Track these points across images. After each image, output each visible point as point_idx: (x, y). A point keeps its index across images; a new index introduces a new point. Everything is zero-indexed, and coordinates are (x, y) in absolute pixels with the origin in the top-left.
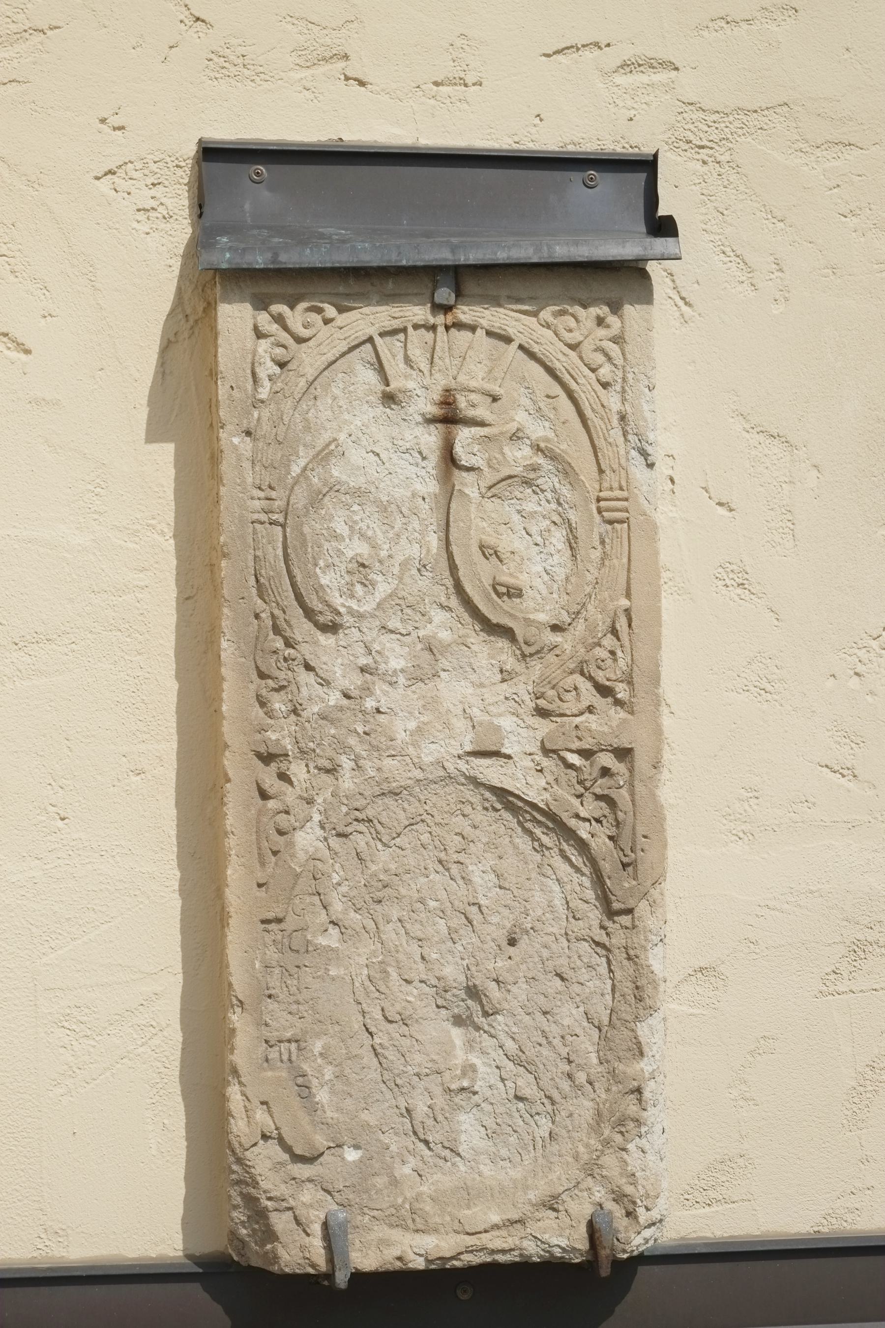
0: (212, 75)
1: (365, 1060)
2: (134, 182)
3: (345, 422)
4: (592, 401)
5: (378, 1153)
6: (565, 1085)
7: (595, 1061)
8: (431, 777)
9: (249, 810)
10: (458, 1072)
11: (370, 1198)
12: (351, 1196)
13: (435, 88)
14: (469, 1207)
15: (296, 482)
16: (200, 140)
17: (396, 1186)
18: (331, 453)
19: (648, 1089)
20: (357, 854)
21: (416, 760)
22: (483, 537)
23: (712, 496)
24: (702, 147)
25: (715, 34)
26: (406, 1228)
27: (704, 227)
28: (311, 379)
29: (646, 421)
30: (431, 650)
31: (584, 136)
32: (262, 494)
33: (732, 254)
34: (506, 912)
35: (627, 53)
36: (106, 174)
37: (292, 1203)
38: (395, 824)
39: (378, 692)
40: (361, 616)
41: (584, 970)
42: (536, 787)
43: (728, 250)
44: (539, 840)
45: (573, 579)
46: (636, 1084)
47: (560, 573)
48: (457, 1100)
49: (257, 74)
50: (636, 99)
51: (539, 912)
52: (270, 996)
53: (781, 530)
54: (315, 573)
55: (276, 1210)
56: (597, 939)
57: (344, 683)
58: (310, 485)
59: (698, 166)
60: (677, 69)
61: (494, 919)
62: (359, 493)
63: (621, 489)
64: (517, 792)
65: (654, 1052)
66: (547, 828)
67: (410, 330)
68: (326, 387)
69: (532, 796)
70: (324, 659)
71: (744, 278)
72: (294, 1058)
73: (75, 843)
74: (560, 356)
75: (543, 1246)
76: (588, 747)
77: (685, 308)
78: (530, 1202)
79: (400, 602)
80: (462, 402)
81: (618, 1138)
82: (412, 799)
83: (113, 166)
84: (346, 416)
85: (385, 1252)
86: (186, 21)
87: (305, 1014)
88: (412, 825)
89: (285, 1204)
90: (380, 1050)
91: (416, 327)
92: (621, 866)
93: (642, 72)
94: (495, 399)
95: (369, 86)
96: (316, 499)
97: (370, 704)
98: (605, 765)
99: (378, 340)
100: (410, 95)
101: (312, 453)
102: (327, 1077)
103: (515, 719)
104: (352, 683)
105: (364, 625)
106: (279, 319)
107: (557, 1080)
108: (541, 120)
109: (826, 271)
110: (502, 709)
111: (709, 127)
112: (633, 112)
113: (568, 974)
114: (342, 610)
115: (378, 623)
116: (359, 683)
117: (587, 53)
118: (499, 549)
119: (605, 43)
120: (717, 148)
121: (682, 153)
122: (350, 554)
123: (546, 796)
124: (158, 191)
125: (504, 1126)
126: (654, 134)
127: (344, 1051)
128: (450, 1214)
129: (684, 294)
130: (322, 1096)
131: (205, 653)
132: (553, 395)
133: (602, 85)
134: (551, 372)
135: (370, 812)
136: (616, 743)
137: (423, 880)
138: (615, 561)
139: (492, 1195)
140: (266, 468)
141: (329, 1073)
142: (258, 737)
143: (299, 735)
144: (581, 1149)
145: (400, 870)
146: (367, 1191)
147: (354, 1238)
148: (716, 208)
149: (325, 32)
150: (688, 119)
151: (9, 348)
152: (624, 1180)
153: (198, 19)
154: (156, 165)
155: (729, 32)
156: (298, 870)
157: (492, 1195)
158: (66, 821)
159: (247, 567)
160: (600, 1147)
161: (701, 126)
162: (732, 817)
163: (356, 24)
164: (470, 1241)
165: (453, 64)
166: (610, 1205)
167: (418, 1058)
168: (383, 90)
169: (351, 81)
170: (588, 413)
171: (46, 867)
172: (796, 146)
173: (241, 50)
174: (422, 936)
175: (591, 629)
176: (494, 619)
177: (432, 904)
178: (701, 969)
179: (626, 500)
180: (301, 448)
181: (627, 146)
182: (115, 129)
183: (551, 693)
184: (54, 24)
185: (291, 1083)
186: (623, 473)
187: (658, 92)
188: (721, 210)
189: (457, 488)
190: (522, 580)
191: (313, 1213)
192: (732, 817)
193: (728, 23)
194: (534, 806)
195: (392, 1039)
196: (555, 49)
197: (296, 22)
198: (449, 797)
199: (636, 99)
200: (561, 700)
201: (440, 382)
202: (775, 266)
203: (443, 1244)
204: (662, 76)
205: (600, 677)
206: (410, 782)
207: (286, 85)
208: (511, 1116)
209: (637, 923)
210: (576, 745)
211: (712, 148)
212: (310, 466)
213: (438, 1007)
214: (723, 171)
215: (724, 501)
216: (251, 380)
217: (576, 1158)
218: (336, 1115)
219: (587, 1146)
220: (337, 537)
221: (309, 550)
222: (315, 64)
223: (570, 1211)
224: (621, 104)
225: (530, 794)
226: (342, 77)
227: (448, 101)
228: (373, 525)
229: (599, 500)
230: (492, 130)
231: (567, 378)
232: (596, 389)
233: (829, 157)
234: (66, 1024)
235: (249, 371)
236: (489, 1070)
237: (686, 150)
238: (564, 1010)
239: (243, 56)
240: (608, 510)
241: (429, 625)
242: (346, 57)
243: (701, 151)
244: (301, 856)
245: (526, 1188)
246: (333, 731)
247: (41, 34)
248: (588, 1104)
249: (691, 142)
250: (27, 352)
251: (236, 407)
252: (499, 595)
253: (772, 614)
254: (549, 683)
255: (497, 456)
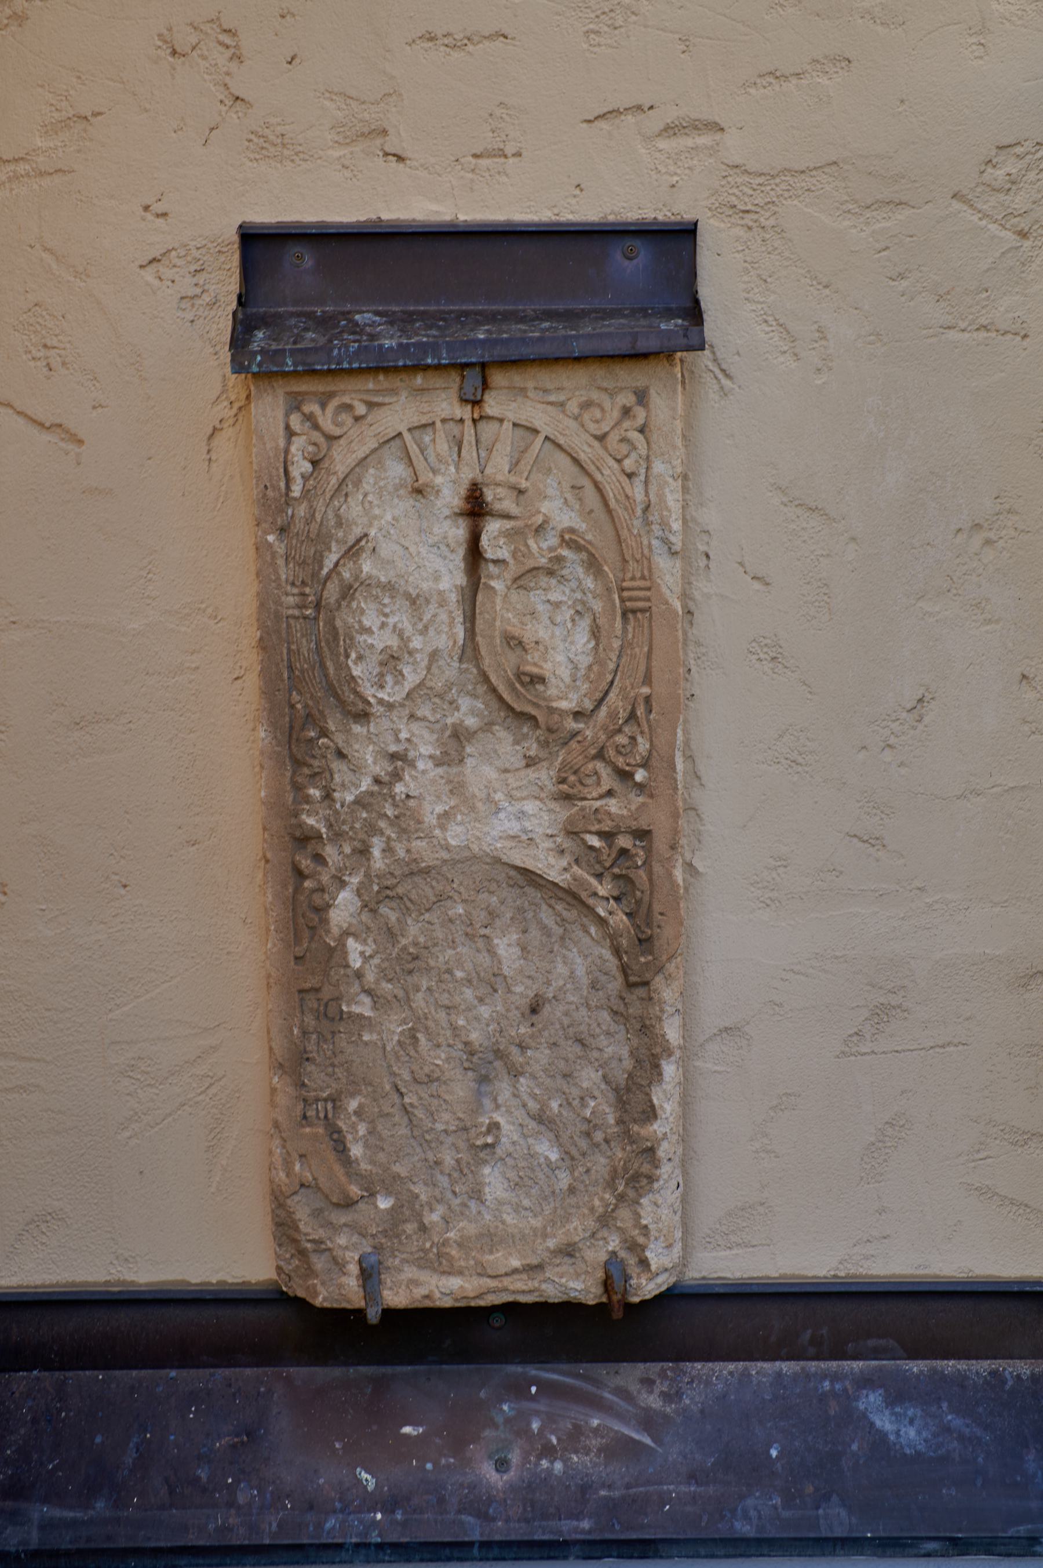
0: (252, 156)
1: (397, 1119)
2: (178, 270)
3: (375, 517)
4: (616, 493)
5: (409, 1202)
6: (583, 1144)
7: (612, 1121)
8: (457, 857)
9: (287, 889)
10: (484, 1129)
11: (400, 1242)
12: (383, 1241)
13: (473, 161)
14: (491, 1252)
15: (328, 577)
16: (240, 227)
17: (425, 1232)
18: (362, 549)
19: (662, 1149)
20: (389, 929)
21: (443, 842)
22: (509, 628)
23: (748, 570)
24: (748, 212)
25: (762, 91)
26: (435, 1270)
27: (747, 295)
28: (341, 476)
29: (670, 511)
30: (458, 737)
31: (625, 205)
32: (295, 591)
33: (774, 323)
34: (529, 982)
35: (671, 115)
36: (150, 262)
37: (329, 1244)
38: (424, 901)
39: (407, 777)
40: (390, 706)
41: (602, 1037)
42: (557, 867)
43: (770, 319)
44: (560, 915)
45: (595, 668)
46: (649, 1144)
47: (585, 661)
48: (482, 1155)
49: (297, 154)
50: (679, 163)
51: (561, 983)
52: (308, 1059)
53: (817, 604)
54: (347, 665)
55: (315, 1251)
56: (615, 1008)
57: (377, 770)
58: (342, 580)
59: (741, 232)
60: (722, 129)
61: (519, 989)
62: (389, 588)
63: (643, 578)
64: (539, 872)
65: (668, 1114)
66: (568, 904)
67: (438, 424)
68: (358, 483)
69: (554, 876)
70: (356, 747)
71: (786, 348)
72: (330, 1115)
73: (136, 909)
74: (586, 448)
75: (560, 1289)
76: (607, 829)
77: (725, 382)
78: (548, 1249)
79: (429, 692)
80: (489, 495)
81: (631, 1194)
82: (440, 877)
83: (157, 254)
84: (377, 511)
85: (415, 1291)
86: (227, 102)
87: (340, 1075)
88: (440, 901)
89: (323, 1246)
90: (410, 1109)
91: (444, 421)
92: (637, 942)
93: (686, 134)
94: (521, 492)
95: (408, 162)
96: (347, 592)
97: (399, 789)
98: (624, 846)
99: (407, 436)
100: (449, 169)
101: (344, 548)
102: (361, 1133)
103: (538, 803)
104: (382, 769)
105: (394, 715)
106: (310, 418)
107: (576, 1138)
108: (582, 190)
109: (872, 338)
110: (525, 793)
111: (754, 190)
112: (676, 178)
113: (589, 1041)
114: (372, 700)
115: (407, 712)
116: (390, 769)
117: (630, 117)
118: (524, 640)
119: (649, 105)
120: (762, 212)
121: (726, 220)
122: (380, 646)
123: (567, 876)
124: (201, 278)
125: (526, 1179)
126: (696, 200)
127: (376, 1110)
128: (474, 1258)
129: (724, 366)
130: (356, 1151)
131: (253, 730)
132: (579, 485)
133: (644, 151)
134: (576, 461)
135: (400, 890)
136: (634, 825)
137: (450, 952)
138: (637, 650)
139: (514, 1242)
140: (299, 565)
141: (362, 1129)
142: (293, 821)
143: (332, 819)
144: (597, 1202)
145: (429, 944)
146: (398, 1236)
147: (387, 1279)
148: (759, 276)
149: (363, 106)
150: (733, 183)
151: (63, 439)
152: (637, 1232)
153: (237, 98)
154: (200, 252)
155: (777, 88)
156: (332, 944)
157: (514, 1242)
158: (128, 888)
159: (282, 660)
160: (614, 1201)
161: (746, 189)
162: (760, 885)
163: (394, 97)
164: (492, 1283)
165: (491, 135)
166: (623, 1254)
167: (446, 1116)
168: (422, 166)
169: (391, 158)
170: (612, 503)
171: (111, 930)
172: (844, 207)
173: (279, 129)
174: (450, 1004)
175: (613, 715)
176: (518, 707)
177: (459, 974)
178: (726, 1029)
179: (649, 589)
180: (333, 544)
181: (669, 214)
182: (158, 216)
183: (572, 778)
184: (97, 110)
185: (327, 1139)
186: (645, 562)
187: (702, 155)
188: (764, 277)
189: (483, 580)
190: (546, 669)
191: (348, 1255)
192: (760, 885)
193: (777, 78)
194: (555, 884)
195: (421, 1099)
196: (596, 115)
197: (334, 97)
198: (475, 876)
199: (679, 163)
200: (582, 784)
201: (467, 475)
202: (817, 335)
203: (467, 1285)
204: (704, 140)
205: (620, 761)
206: (439, 862)
207: (325, 164)
208: (533, 1170)
209: (653, 995)
210: (596, 827)
211: (756, 212)
212: (342, 562)
213: (465, 1069)
214: (768, 236)
215: (760, 575)
216: (283, 478)
217: (592, 1209)
218: (369, 1167)
219: (602, 1199)
220: (369, 631)
221: (342, 643)
222: (353, 141)
223: (586, 1258)
224: (664, 170)
225: (552, 874)
226: (381, 154)
227: (487, 174)
228: (401, 618)
229: (623, 590)
230: (532, 203)
231: (591, 468)
232: (621, 480)
233: (879, 218)
234: (131, 1074)
235: (282, 470)
236: (512, 1128)
237: (730, 216)
238: (583, 1073)
239: (283, 135)
240: (630, 599)
241: (456, 714)
242: (385, 132)
243: (746, 215)
244: (335, 931)
245: (545, 1236)
246: (364, 815)
247: (85, 122)
248: (603, 1161)
249: (735, 206)
250: (81, 442)
251: (270, 506)
252: (522, 684)
253: (804, 687)
254: (571, 768)
255: (522, 548)
